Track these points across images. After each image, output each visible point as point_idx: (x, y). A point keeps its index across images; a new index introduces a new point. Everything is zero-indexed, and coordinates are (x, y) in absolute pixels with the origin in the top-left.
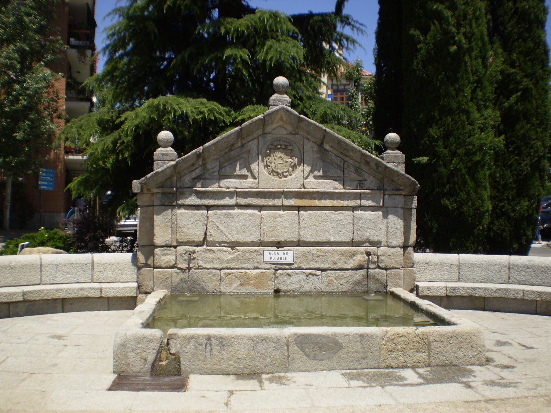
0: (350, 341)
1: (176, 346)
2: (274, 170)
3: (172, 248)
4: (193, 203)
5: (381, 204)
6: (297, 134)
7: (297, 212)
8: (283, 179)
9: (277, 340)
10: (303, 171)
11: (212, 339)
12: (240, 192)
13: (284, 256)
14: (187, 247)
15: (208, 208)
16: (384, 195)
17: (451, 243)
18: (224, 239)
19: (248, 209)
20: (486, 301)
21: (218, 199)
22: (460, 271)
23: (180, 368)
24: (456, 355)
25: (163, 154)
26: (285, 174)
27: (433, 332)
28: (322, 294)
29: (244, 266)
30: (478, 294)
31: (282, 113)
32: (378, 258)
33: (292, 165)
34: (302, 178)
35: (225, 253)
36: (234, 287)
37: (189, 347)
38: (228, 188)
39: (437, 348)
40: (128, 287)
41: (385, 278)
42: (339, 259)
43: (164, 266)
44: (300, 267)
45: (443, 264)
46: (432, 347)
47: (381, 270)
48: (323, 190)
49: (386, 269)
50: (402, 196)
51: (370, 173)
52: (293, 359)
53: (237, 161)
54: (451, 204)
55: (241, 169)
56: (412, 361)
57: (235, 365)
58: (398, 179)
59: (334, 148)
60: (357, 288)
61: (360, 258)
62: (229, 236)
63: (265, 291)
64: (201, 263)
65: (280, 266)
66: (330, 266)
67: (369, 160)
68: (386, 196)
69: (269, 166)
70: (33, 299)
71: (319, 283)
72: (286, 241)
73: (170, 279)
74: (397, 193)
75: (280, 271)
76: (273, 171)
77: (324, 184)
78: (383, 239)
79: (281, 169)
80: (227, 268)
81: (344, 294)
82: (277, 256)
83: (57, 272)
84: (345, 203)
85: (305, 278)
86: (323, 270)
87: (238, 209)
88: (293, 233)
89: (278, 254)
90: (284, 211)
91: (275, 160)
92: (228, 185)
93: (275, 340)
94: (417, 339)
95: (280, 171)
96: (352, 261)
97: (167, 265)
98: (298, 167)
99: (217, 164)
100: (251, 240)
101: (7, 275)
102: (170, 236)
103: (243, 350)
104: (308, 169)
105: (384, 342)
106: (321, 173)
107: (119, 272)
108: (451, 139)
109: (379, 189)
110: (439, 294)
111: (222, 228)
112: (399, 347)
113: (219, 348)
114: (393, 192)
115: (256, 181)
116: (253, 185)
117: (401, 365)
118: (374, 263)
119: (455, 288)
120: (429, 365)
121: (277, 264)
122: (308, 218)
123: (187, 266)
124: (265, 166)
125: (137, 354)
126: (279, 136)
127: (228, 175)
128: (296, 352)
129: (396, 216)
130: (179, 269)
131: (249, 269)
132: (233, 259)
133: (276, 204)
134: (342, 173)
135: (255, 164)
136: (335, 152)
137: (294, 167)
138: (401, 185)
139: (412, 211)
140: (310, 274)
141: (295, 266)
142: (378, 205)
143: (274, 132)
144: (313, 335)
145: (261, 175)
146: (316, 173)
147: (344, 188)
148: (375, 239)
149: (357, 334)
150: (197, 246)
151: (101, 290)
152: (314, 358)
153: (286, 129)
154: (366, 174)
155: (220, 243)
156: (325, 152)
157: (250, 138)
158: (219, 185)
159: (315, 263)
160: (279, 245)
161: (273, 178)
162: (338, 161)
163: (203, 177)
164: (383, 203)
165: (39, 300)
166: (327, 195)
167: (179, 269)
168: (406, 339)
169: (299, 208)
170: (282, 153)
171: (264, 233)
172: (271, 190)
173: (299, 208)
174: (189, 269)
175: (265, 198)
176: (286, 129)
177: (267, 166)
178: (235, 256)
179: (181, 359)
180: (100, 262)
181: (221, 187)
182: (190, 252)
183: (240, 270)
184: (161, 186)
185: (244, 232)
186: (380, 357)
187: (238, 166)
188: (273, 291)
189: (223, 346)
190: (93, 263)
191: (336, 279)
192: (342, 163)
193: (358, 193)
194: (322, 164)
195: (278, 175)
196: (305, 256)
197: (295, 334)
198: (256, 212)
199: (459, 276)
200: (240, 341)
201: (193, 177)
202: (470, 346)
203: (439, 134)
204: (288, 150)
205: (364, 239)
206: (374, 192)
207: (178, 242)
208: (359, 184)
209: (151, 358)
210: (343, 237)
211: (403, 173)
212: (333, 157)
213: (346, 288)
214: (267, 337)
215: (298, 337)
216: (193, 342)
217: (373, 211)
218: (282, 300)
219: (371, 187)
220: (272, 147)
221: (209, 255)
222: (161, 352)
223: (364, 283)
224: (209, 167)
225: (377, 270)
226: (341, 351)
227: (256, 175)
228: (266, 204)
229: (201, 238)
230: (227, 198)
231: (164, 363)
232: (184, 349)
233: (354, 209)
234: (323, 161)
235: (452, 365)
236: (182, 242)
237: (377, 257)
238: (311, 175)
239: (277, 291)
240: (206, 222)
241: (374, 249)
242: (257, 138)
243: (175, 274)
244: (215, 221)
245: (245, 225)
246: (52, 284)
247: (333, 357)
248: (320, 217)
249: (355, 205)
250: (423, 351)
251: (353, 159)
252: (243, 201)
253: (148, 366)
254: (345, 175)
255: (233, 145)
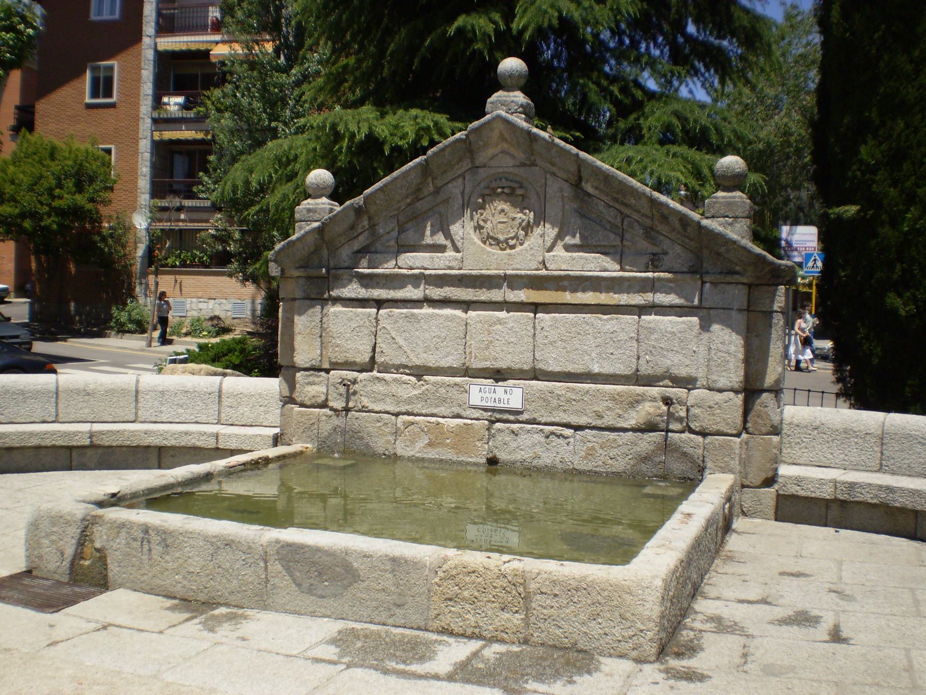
0: (373, 568)
1: (101, 537)
2: (491, 234)
3: (323, 374)
4: (353, 295)
5: (696, 302)
6: (533, 164)
7: (532, 315)
8: (508, 251)
9: (248, 548)
10: (542, 236)
11: (150, 531)
12: (430, 275)
13: (506, 397)
14: (344, 373)
15: (380, 304)
16: (703, 283)
17: (907, 389)
18: (404, 360)
19: (447, 307)
20: (920, 520)
21: (394, 288)
22: (884, 449)
23: (106, 575)
24: (584, 629)
25: (309, 210)
26: (512, 242)
27: (538, 574)
28: (573, 474)
29: (435, 411)
30: (899, 501)
31: (499, 126)
32: (688, 410)
33: (524, 224)
34: (544, 250)
35: (405, 386)
36: (418, 449)
37: (118, 541)
38: (411, 269)
39: (545, 608)
40: (260, 435)
41: (701, 451)
42: (609, 409)
43: (309, 403)
44: (535, 419)
45: (847, 433)
46: (533, 605)
47: (692, 436)
48: (578, 273)
49: (704, 434)
50: (740, 286)
51: (673, 238)
52: (274, 587)
53: (425, 220)
54: (905, 305)
55: (433, 233)
56: (490, 627)
57: (185, 582)
58: (728, 251)
59: (601, 191)
60: (644, 467)
61: (650, 409)
62: (411, 356)
63: (470, 460)
64: (366, 401)
65: (498, 416)
66: (590, 421)
67: (666, 212)
68: (707, 285)
69: (483, 228)
70: (107, 444)
71: (569, 452)
72: (509, 368)
73: (316, 426)
74: (729, 278)
75: (498, 425)
76: (489, 237)
77: (583, 261)
78: (700, 373)
79: (503, 234)
80: (408, 413)
81: (615, 478)
82: (493, 396)
83: (163, 405)
84: (624, 299)
85: (543, 440)
86: (578, 428)
87: (429, 307)
88: (522, 354)
89: (494, 392)
90: (508, 312)
91: (493, 215)
92: (410, 264)
93: (245, 549)
94: (502, 582)
95: (501, 237)
96: (634, 414)
97: (313, 401)
98: (535, 229)
99: (393, 224)
100: (448, 365)
101: (80, 405)
102: (319, 352)
103: (197, 559)
104: (551, 232)
105: (437, 580)
106: (577, 240)
107: (262, 409)
108: (906, 166)
109: (693, 271)
110: (818, 494)
111: (401, 342)
112: (466, 594)
113: (160, 548)
114: (721, 278)
115: (459, 255)
116: (454, 264)
117: (469, 631)
118: (680, 420)
119: (852, 486)
120: (526, 642)
121: (493, 410)
122: (551, 326)
123: (344, 405)
124: (475, 228)
125: (53, 542)
126: (501, 170)
127: (413, 246)
128: (279, 575)
129: (729, 326)
130: (332, 409)
131: (444, 417)
132: (417, 397)
133: (493, 299)
134: (619, 239)
135: (457, 225)
136: (605, 198)
137: (528, 228)
138: (737, 264)
139: (772, 318)
140: (552, 433)
141: (525, 417)
142: (689, 304)
143: (492, 163)
144: (308, 546)
145: (472, 243)
146: (568, 240)
147: (622, 269)
148: (683, 372)
149: (386, 556)
150: (360, 371)
151: (217, 436)
152: (310, 591)
153: (513, 156)
154: (667, 241)
155: (399, 368)
156: (586, 198)
157: (450, 176)
158: (396, 264)
159: (562, 414)
160: (499, 375)
161: (489, 249)
162: (610, 215)
163: (373, 249)
164: (701, 300)
165: (117, 446)
166: (588, 283)
167: (332, 409)
168: (479, 580)
169: (536, 308)
170: (506, 202)
171: (471, 353)
172: (483, 272)
173: (536, 308)
174: (347, 410)
175: (474, 287)
176: (513, 156)
177: (478, 228)
178: (420, 392)
179: (109, 561)
180: (231, 390)
181: (399, 268)
182: (349, 381)
183: (429, 419)
184: (304, 265)
185: (437, 349)
186: (428, 608)
187: (429, 228)
188: (484, 460)
189: (167, 546)
190: (220, 391)
191: (602, 448)
192: (619, 219)
193: (648, 278)
194: (579, 221)
195: (498, 244)
196: (544, 399)
197: (278, 541)
198: (458, 313)
199: (881, 460)
200: (192, 542)
201: (355, 249)
202: (617, 614)
203: (879, 156)
204: (516, 194)
205: (659, 371)
206: (679, 276)
207: (331, 363)
208: (652, 261)
209: (70, 551)
210: (618, 365)
211: (338, 208)
212: (601, 208)
213: (620, 465)
214: (233, 541)
215: (282, 547)
216: (123, 534)
217: (681, 316)
218: (501, 478)
219: (677, 266)
220: (487, 192)
221: (379, 387)
222: (83, 545)
223: (657, 459)
224: (381, 231)
225: (686, 435)
226: (356, 585)
227: (459, 244)
228: (475, 298)
229: (366, 358)
230: (410, 286)
231: (87, 563)
232: (112, 543)
233: (641, 310)
234: (583, 216)
235: (574, 647)
236: (336, 363)
237: (684, 408)
238: (560, 244)
239: (493, 461)
240: (374, 329)
241: (681, 392)
242: (463, 176)
243: (324, 418)
244: (388, 327)
245: (439, 337)
246: (155, 422)
247: (342, 594)
248: (575, 325)
249: (643, 302)
250: (515, 609)
251: (638, 211)
252: (436, 293)
253: (66, 564)
254: (625, 243)
255: (419, 190)
